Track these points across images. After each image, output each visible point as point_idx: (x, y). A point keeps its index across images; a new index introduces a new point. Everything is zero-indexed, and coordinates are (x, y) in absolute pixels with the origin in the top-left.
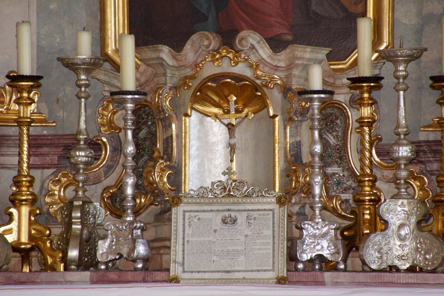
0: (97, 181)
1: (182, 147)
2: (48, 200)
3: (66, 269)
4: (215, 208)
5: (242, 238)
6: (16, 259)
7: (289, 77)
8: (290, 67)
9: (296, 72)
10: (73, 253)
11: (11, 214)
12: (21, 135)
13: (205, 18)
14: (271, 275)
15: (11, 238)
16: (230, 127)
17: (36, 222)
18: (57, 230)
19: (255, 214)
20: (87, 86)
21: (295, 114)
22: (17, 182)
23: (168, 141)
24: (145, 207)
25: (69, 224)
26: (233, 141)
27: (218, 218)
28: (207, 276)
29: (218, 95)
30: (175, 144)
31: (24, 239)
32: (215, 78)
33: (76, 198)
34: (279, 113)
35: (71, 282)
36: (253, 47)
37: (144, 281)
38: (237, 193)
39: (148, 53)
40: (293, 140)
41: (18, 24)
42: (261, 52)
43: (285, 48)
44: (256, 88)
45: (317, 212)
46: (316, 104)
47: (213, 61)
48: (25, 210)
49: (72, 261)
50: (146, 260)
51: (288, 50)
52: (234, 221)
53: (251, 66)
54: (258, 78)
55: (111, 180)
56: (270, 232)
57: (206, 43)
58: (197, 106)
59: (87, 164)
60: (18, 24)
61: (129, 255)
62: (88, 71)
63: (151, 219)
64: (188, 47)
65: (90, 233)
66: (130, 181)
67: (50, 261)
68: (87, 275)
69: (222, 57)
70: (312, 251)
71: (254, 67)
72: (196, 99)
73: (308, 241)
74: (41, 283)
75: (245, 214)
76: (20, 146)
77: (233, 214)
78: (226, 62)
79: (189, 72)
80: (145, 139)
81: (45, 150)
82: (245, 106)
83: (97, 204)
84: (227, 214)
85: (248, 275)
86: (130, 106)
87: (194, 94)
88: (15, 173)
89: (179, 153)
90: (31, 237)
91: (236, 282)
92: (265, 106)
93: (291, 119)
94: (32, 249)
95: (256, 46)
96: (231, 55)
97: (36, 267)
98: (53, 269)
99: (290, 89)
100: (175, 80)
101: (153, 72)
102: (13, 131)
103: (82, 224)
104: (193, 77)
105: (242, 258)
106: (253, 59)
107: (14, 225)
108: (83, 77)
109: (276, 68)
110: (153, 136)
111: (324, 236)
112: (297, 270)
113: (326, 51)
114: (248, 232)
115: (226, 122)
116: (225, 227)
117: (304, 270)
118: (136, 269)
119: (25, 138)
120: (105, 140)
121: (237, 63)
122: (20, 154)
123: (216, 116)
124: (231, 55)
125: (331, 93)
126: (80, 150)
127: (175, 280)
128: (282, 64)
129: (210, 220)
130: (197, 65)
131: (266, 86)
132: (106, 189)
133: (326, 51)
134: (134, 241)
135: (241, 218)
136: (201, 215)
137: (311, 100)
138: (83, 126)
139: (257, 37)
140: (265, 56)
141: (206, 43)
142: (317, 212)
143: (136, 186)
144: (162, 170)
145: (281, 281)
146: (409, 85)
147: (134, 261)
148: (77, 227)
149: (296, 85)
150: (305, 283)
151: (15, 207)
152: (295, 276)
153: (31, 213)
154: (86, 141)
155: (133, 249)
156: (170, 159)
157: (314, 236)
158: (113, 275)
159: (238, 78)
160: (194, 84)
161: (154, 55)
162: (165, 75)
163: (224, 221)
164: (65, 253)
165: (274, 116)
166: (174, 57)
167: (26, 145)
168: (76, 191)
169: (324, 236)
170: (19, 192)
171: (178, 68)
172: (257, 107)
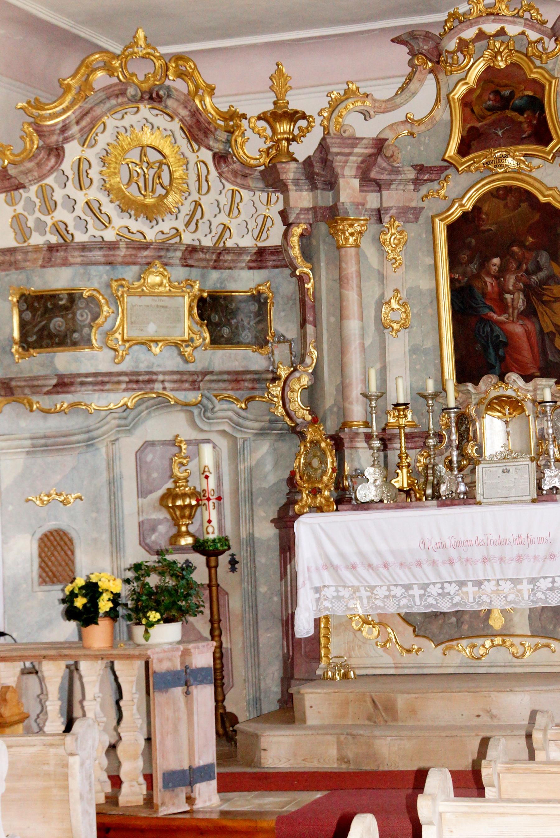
0: (442, 454)
1: (482, 434)
2: (418, 465)
3: (426, 499)
4: (499, 465)
5: (513, 480)
6: (403, 495)
7: (535, 395)
8: (535, 390)
9: (538, 392)
10: (429, 491)
11: (398, 474)
12: (400, 433)
13: (493, 367)
14: (529, 498)
15: (397, 485)
16: (507, 422)
17: (410, 476)
18: (422, 480)
19: (519, 467)
20: (432, 406)
21: (540, 413)
22: (400, 457)
23: (475, 432)
24: (465, 466)
25: (427, 477)
26: (508, 429)
27: (500, 471)
28: (495, 500)
29: (499, 406)
30: (478, 433)
31: (405, 485)
32: (496, 398)
33: (430, 463)
34: (531, 414)
35: (428, 507)
36: (514, 381)
37: (464, 504)
38: (509, 457)
39: (462, 387)
40: (540, 427)
41: (396, 378)
42: (519, 383)
43: (531, 380)
44: (518, 402)
45: (552, 464)
46: (548, 408)
47: (495, 388)
48: (405, 470)
49: (429, 496)
50: (465, 493)
51: (533, 381)
52: (509, 471)
53: (514, 390)
54: (518, 396)
55: (447, 454)
56: (527, 476)
57: (490, 380)
58: (489, 412)
59: (434, 446)
60: (396, 378)
61: (456, 491)
62: (432, 399)
63: (469, 472)
64: (481, 383)
65: (438, 481)
66: (455, 453)
67: (418, 495)
68: (435, 502)
69: (499, 387)
70: (550, 484)
71: (516, 391)
72: (487, 409)
73: (547, 479)
74: (413, 508)
75: (514, 467)
76: (400, 439)
77: (508, 468)
78: (501, 389)
79: (483, 396)
80: (464, 431)
81: (416, 439)
82: (514, 411)
83: (441, 466)
84: (504, 468)
85: (517, 499)
86: (453, 415)
87: (487, 407)
88: (398, 452)
89: (481, 437)
90: (409, 485)
91: (511, 503)
92: (524, 411)
93: (537, 417)
94: (410, 490)
95: (517, 380)
96: (503, 386)
97: (414, 499)
98: (420, 499)
99: (536, 401)
100: (477, 400)
101: (99, 398)
102: (397, 431)
103: (433, 476)
104: (485, 398)
105: (513, 490)
106: (515, 387)
107: (399, 478)
108: (430, 402)
109: (528, 391)
110: (468, 430)
111: (556, 476)
112: (542, 494)
113: (554, 380)
114: (516, 477)
115: (504, 420)
116: (504, 474)
117: (546, 494)
118: (460, 498)
119: (403, 435)
120: (444, 432)
121: (507, 390)
122: (400, 443)
123: (499, 417)
124: (503, 386)
125: (556, 402)
126: (431, 439)
127: (480, 503)
128: (531, 388)
129: (496, 471)
130: (486, 392)
131: (523, 400)
132: (447, 458)
133: (554, 380)
134: (458, 484)
135: (512, 470)
136: (491, 469)
137: (545, 406)
138: (431, 426)
139: (517, 375)
140: (521, 385)
141: (490, 380)
142: (552, 464)
143: (458, 456)
144: (472, 447)
145: (534, 501)
146: (197, 361)
147: (459, 494)
148: (431, 478)
149: (539, 399)
150: (546, 501)
151: (399, 469)
152: (541, 498)
153: (408, 472)
154: (433, 434)
155: (457, 489)
156: (476, 441)
157: (551, 476)
158: (449, 502)
159: (509, 397)
160: (486, 402)
161: (465, 388)
162: (471, 398)
163: (503, 472)
164: (425, 492)
165: (529, 416)
166: (475, 389)
167: (403, 438)
168: (430, 460)
169: (556, 476)
170: (401, 462)
171: (478, 394)
172: (520, 411)
